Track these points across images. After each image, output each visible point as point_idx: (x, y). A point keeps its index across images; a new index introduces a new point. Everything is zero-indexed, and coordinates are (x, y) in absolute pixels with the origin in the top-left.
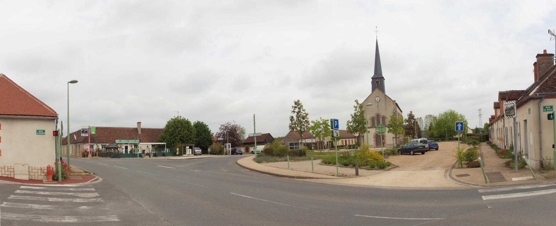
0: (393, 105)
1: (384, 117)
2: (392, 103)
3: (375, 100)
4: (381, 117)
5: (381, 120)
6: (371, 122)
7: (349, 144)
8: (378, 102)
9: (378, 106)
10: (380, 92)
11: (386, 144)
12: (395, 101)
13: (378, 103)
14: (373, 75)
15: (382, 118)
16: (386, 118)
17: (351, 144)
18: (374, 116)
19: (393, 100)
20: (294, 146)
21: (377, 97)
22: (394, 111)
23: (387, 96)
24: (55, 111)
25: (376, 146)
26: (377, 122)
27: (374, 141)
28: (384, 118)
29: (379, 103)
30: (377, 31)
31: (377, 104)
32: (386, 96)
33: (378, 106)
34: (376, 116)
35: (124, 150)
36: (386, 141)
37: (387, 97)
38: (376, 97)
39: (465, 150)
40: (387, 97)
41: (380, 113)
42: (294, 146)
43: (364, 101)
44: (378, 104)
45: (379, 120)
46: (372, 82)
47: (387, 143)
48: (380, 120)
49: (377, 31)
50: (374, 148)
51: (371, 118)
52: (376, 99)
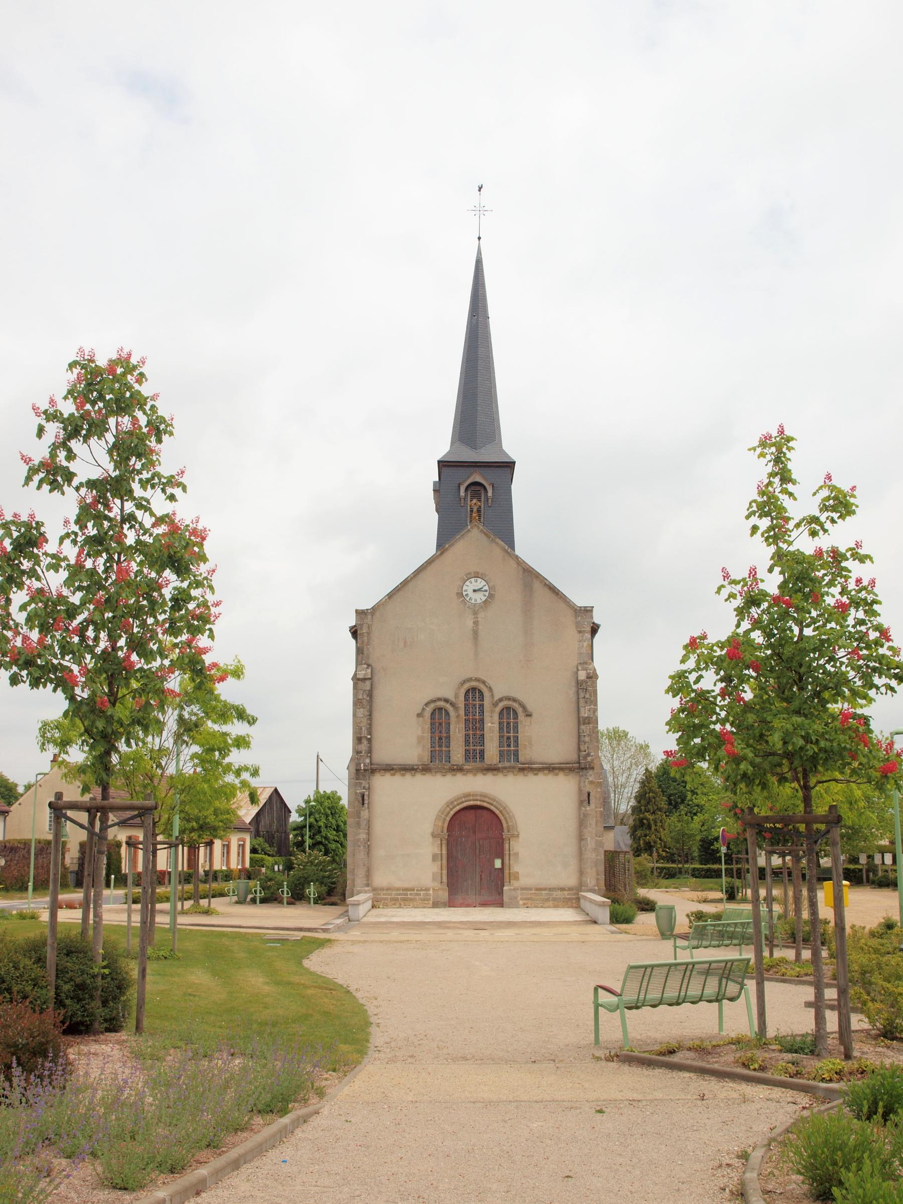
0: (577, 636)
1: (515, 705)
2: (568, 619)
3: (460, 595)
4: (495, 705)
5: (491, 725)
6: (428, 735)
7: (207, 868)
8: (476, 610)
9: (476, 633)
10: (497, 550)
11: (516, 884)
12: (588, 611)
13: (475, 613)
14: (504, 448)
15: (498, 709)
16: (529, 715)
17: (217, 866)
18: (451, 697)
19: (580, 602)
20: (723, 867)
21: (477, 575)
22: (582, 675)
23: (538, 576)
24: (838, 486)
25: (444, 895)
26: (467, 736)
27: (434, 858)
28: (447, 713)
29: (481, 615)
30: (480, 211)
31: (470, 623)
32: (529, 575)
33: (476, 633)
34: (462, 698)
35: (801, 807)
36: (516, 868)
37: (537, 585)
38: (469, 577)
39: (48, 951)
40: (537, 585)
41: (491, 682)
42: (723, 867)
43: (391, 595)
44: (476, 623)
45: (482, 721)
46: (438, 490)
47: (524, 881)
48: (488, 725)
49: (480, 211)
50: (436, 905)
51: (429, 710)
52: (470, 586)
